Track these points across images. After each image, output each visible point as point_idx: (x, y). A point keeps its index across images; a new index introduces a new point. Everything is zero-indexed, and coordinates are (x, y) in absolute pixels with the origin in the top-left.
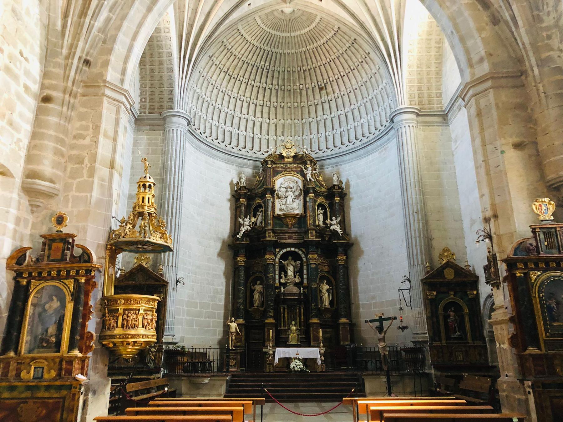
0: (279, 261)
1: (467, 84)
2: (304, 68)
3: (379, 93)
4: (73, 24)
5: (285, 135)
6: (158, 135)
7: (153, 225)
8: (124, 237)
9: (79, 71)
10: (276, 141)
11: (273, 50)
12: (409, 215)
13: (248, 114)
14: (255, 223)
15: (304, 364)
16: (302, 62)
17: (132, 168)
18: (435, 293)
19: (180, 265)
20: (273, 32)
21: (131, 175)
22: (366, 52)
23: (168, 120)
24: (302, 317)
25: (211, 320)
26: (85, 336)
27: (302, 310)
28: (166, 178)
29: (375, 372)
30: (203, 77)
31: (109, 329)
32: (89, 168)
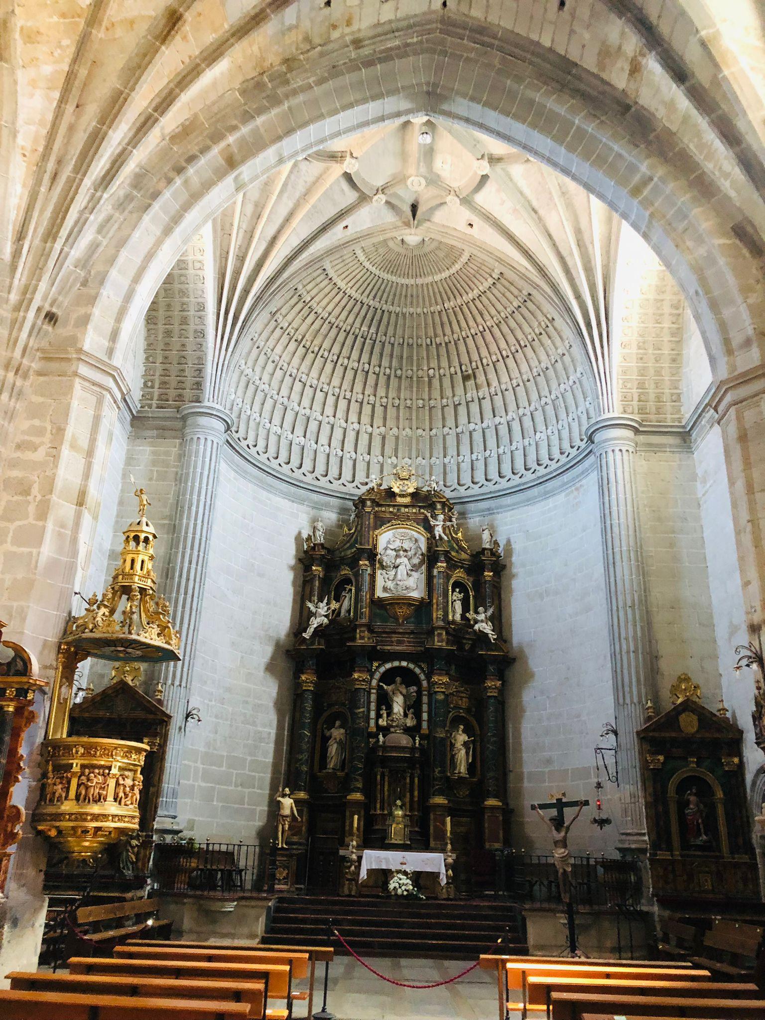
0: (378, 685)
1: (722, 383)
2: (438, 340)
3: (568, 388)
4: (32, 252)
5: (400, 455)
6: (171, 447)
7: (147, 611)
8: (91, 631)
9: (36, 330)
10: (382, 466)
11: (385, 307)
12: (618, 610)
13: (334, 416)
14: (335, 612)
15: (416, 883)
17: (121, 503)
18: (661, 758)
19: (195, 684)
20: (386, 276)
21: (117, 516)
23: (190, 421)
24: (416, 793)
25: (247, 790)
26: (7, 813)
27: (416, 780)
28: (181, 524)
29: (546, 905)
30: (258, 347)
31: (51, 801)
32: (40, 501)
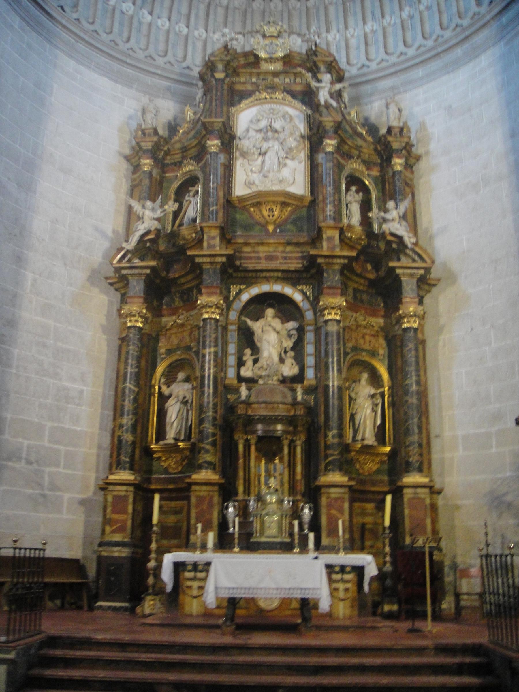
24: (299, 469)
27: (299, 450)
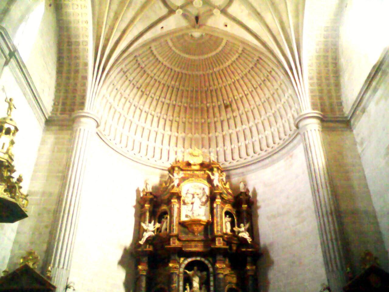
16: (209, 82)
22: (267, 71)
